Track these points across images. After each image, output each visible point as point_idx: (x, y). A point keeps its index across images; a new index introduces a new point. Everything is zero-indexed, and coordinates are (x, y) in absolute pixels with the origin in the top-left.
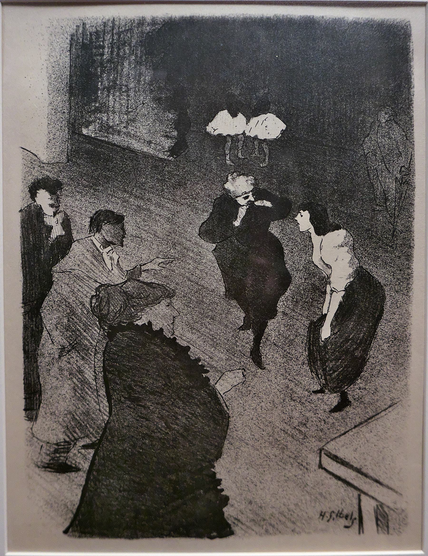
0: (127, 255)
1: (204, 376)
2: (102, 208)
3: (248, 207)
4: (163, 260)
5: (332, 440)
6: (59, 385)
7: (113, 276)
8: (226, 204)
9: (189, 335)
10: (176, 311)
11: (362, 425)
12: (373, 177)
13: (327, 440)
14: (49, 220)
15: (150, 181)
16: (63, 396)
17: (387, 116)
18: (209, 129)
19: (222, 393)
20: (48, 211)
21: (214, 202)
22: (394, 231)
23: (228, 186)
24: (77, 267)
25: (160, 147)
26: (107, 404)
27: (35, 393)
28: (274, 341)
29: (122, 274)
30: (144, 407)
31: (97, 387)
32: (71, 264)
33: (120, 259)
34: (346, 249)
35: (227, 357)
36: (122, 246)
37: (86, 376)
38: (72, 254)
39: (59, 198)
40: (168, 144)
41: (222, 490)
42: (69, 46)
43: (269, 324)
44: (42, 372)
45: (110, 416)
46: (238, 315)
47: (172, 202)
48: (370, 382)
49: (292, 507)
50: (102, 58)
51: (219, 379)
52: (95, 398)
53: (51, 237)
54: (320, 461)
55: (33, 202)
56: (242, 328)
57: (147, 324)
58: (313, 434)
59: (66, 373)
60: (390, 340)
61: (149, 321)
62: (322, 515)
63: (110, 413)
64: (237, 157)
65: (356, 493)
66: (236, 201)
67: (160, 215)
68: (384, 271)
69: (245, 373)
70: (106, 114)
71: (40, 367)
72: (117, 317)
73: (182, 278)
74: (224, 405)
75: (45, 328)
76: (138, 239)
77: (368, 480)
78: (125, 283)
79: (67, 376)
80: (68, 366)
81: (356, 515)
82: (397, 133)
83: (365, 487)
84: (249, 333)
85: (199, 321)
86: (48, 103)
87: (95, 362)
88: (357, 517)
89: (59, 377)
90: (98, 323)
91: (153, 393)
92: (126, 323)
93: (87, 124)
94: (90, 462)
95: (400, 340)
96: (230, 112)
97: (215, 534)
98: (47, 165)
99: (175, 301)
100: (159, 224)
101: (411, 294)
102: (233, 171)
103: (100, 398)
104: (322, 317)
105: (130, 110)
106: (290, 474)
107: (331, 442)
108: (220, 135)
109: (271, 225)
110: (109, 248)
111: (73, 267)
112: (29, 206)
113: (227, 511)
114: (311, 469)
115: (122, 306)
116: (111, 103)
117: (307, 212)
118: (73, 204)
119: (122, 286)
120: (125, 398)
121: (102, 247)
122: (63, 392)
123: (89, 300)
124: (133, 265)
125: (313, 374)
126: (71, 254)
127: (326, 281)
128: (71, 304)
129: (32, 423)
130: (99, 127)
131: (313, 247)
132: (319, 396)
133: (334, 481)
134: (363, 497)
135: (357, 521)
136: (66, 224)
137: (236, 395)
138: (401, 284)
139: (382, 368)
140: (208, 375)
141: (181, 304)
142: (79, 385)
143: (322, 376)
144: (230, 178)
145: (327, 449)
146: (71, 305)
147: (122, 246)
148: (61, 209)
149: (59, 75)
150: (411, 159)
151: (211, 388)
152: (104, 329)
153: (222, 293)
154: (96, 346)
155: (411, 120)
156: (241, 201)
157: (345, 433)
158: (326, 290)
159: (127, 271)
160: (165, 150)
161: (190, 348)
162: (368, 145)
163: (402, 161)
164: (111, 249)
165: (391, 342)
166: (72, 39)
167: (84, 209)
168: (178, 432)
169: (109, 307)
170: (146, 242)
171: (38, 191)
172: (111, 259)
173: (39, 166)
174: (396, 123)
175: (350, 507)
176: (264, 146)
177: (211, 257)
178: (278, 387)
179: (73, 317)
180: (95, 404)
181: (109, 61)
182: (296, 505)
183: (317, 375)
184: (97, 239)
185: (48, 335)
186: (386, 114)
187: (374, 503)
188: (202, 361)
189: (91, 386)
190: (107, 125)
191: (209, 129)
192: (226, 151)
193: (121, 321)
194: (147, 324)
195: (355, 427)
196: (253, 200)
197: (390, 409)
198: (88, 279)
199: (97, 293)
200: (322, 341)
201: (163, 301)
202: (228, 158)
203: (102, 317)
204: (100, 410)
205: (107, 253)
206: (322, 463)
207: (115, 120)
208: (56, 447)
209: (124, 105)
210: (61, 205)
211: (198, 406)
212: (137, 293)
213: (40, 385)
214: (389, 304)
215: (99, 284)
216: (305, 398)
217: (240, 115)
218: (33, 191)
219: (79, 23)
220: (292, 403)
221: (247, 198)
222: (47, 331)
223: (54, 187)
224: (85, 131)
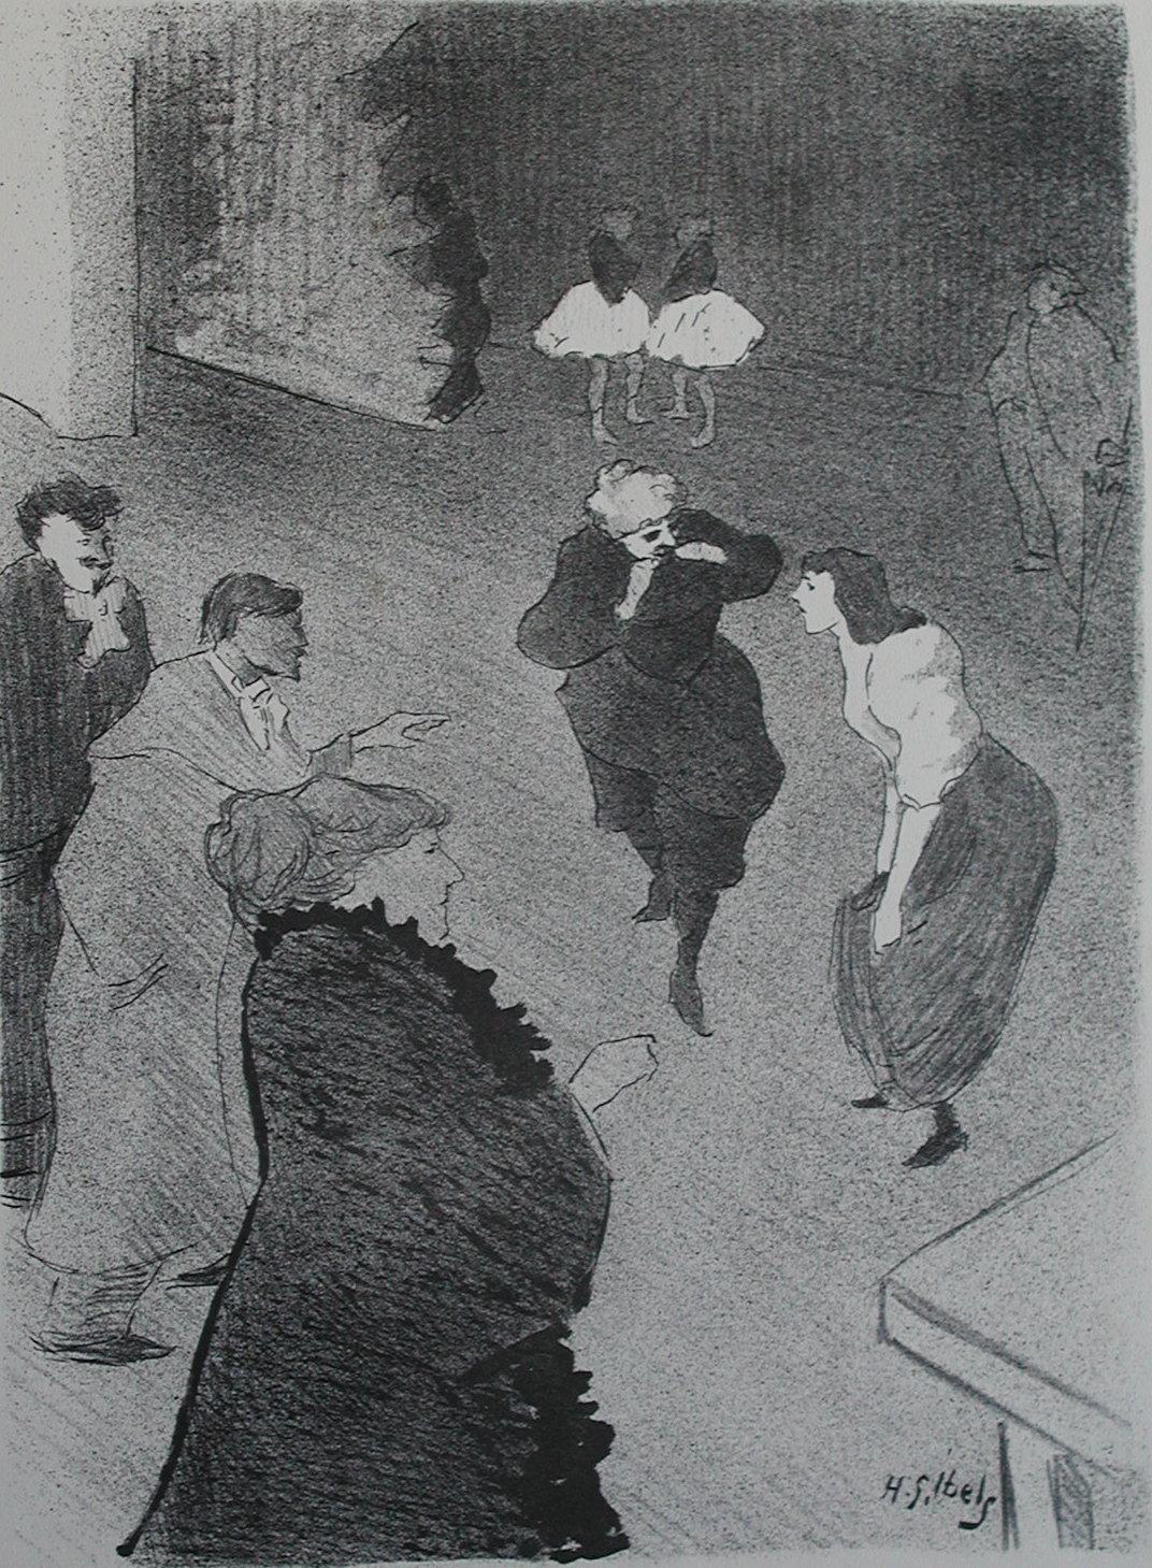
0: (312, 704)
1: (537, 1059)
2: (236, 571)
3: (656, 563)
4: (416, 719)
5: (915, 1253)
6: (110, 1095)
7: (270, 767)
8: (595, 560)
9: (492, 936)
10: (454, 868)
11: (1005, 1209)
12: (1017, 472)
13: (900, 1255)
14: (80, 606)
15: (374, 491)
16: (123, 1128)
17: (1055, 295)
18: (543, 338)
19: (589, 1108)
20: (78, 577)
21: (560, 550)
22: (1081, 630)
23: (598, 502)
24: (164, 742)
25: (403, 391)
26: (254, 1147)
27: (34, 1122)
28: (739, 952)
29: (298, 760)
30: (360, 1152)
31: (223, 1095)
32: (146, 733)
33: (290, 716)
34: (941, 681)
35: (604, 1001)
36: (298, 679)
37: (192, 1063)
38: (149, 705)
39: (110, 539)
40: (429, 381)
41: (594, 1406)
42: (131, 93)
43: (721, 902)
44: (60, 1059)
45: (263, 1184)
46: (631, 875)
47: (437, 550)
48: (1022, 1076)
49: (801, 1461)
50: (226, 132)
51: (581, 1066)
52: (218, 1130)
53: (88, 654)
54: (882, 1317)
55: (32, 551)
56: (643, 916)
57: (370, 907)
58: (859, 1233)
59: (133, 1058)
60: (1077, 949)
61: (377, 898)
62: (893, 1487)
63: (263, 1171)
64: (625, 418)
65: (992, 1419)
66: (623, 545)
67: (404, 589)
68: (1053, 746)
69: (655, 1048)
70: (244, 296)
71: (51, 1043)
72: (285, 888)
73: (470, 772)
74: (595, 1143)
75: (68, 926)
76: (343, 657)
77: (1025, 1379)
78: (305, 786)
79: (135, 1066)
80: (138, 1035)
81: (993, 1488)
82: (1084, 341)
83: (1018, 1403)
84: (666, 928)
85: (521, 886)
86: (72, 261)
87: (217, 1020)
88: (997, 1493)
89: (111, 1069)
90: (226, 905)
91: (388, 1111)
92: (308, 903)
93: (191, 324)
94: (202, 1324)
95: (1103, 946)
96: (602, 288)
97: (572, 1545)
98: (72, 442)
99: (450, 837)
100: (403, 615)
101: (1136, 815)
102: (612, 459)
103: (234, 1130)
104: (875, 880)
105: (313, 283)
106: (795, 1360)
107: (913, 1258)
108: (572, 357)
109: (724, 616)
110: (260, 686)
111: (153, 743)
112: (18, 564)
113: (607, 1474)
114: (857, 1343)
115: (296, 856)
116: (259, 264)
117: (826, 575)
118: (152, 557)
119: (297, 796)
120: (307, 1127)
121: (237, 682)
122: (125, 1114)
123: (201, 837)
124: (330, 734)
125: (853, 1050)
126: (146, 703)
127: (885, 773)
128: (147, 850)
129: (28, 1213)
130: (225, 333)
131: (845, 678)
132: (873, 1118)
133: (924, 1381)
134: (1013, 1431)
135: (996, 1507)
136: (134, 619)
137: (630, 1116)
138: (1107, 783)
139: (1056, 1033)
140: (546, 1054)
141: (468, 846)
142: (172, 1093)
143: (878, 1056)
144: (604, 479)
145: (901, 1281)
146: (146, 854)
147: (298, 679)
148: (116, 571)
149: (103, 178)
150: (1129, 419)
151: (556, 1093)
152: (246, 925)
153: (585, 813)
154: (222, 973)
155: (1128, 303)
156: (637, 546)
157: (952, 1233)
158: (884, 802)
159: (312, 752)
160: (419, 399)
161: (495, 975)
162: (1004, 376)
163: (1104, 425)
164: (265, 687)
165: (1079, 957)
166: (138, 72)
167: (184, 571)
168: (462, 1229)
169: (260, 858)
170: (366, 668)
171: (44, 520)
172: (265, 716)
173: (48, 446)
174: (1085, 314)
175: (976, 1466)
176: (701, 384)
177: (553, 707)
178: (752, 1091)
179: (154, 889)
180: (218, 1148)
181: (247, 138)
182: (814, 1455)
183: (865, 1053)
184: (224, 659)
185: (78, 944)
186: (1053, 287)
187: (1048, 1452)
188: (529, 1013)
189: (206, 1092)
190: (248, 327)
191: (543, 338)
192: (593, 403)
193: (294, 899)
194: (370, 907)
195: (984, 1212)
196: (672, 542)
197: (1085, 1159)
198: (196, 776)
199: (223, 817)
200: (877, 953)
201: (417, 838)
202: (597, 421)
203: (238, 887)
204: (232, 1166)
205: (254, 700)
206: (889, 1323)
207: (267, 312)
208: (101, 1284)
209: (295, 268)
210: (115, 559)
211: (521, 1149)
212: (341, 817)
213: (53, 1095)
214: (1071, 842)
215: (231, 792)
216: (832, 1124)
217: (631, 297)
218: (31, 520)
219: (156, 22)
220: (794, 1138)
221: (652, 536)
222: (76, 932)
223: (92, 508)
224: (183, 346)
